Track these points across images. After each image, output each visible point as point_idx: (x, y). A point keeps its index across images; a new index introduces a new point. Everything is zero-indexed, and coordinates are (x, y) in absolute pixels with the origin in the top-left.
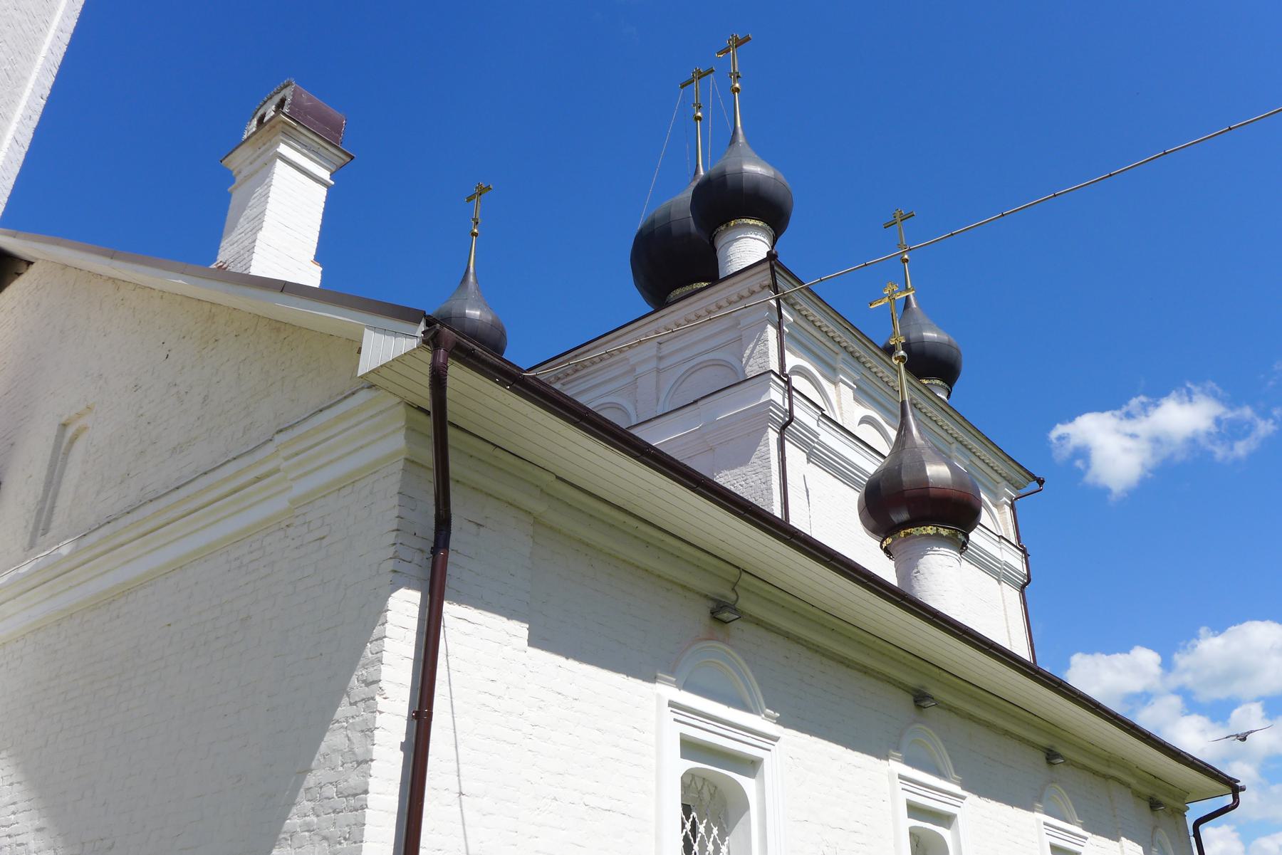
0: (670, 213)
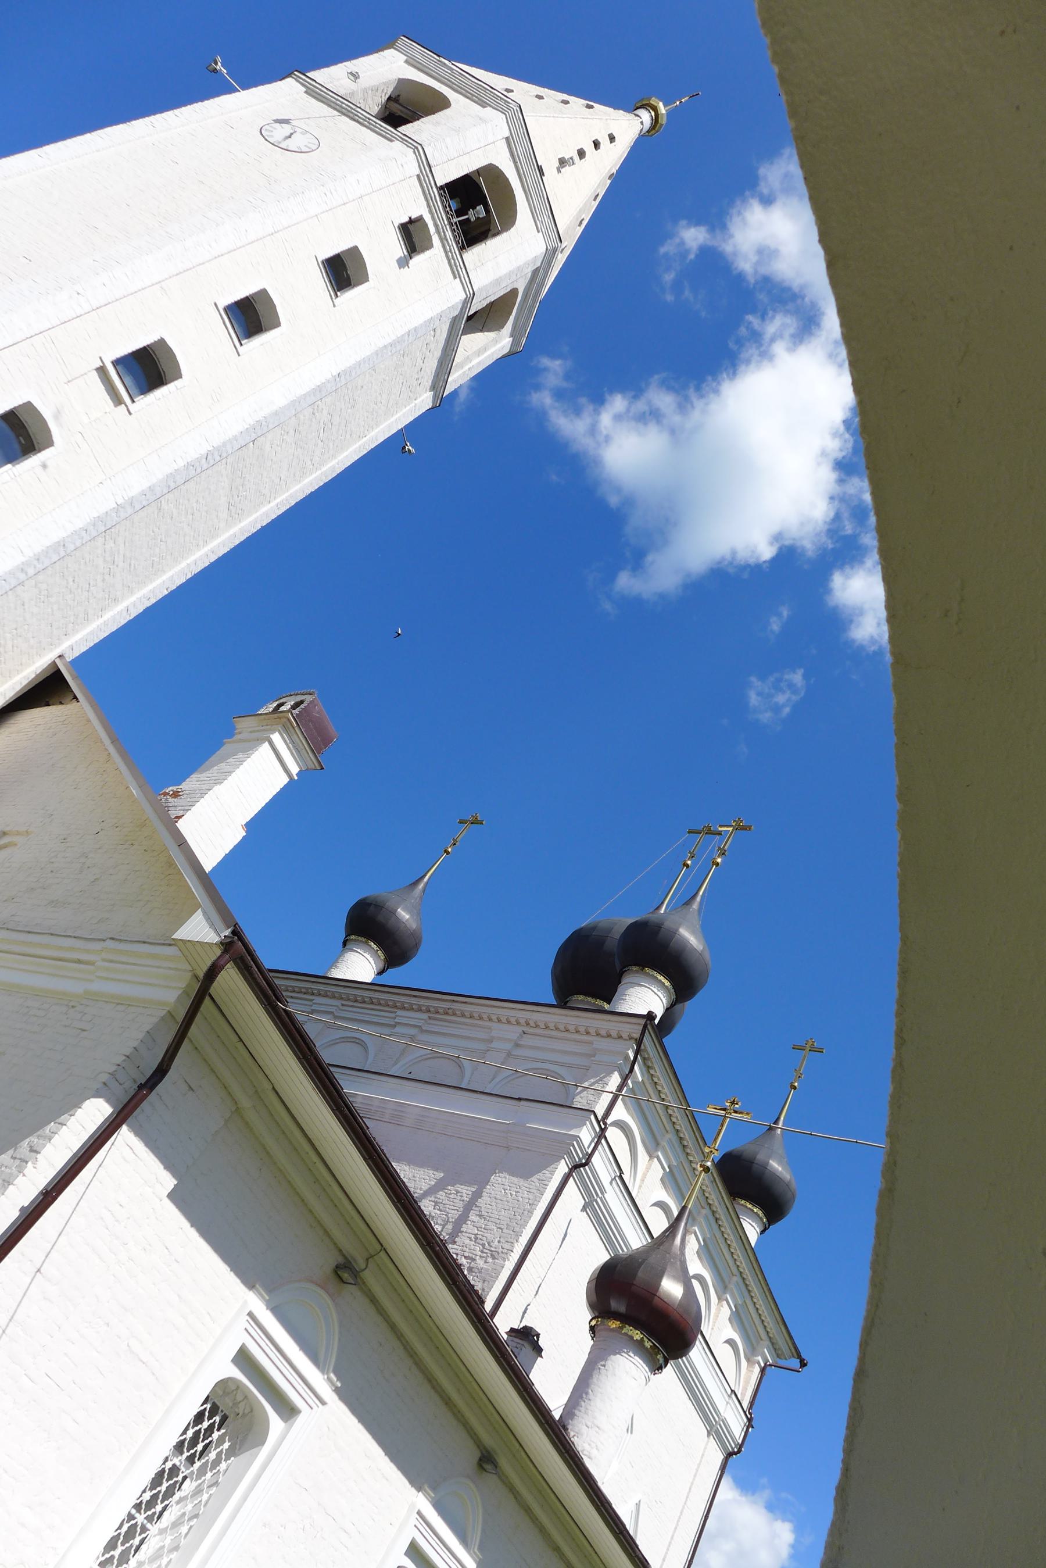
0: (612, 928)
